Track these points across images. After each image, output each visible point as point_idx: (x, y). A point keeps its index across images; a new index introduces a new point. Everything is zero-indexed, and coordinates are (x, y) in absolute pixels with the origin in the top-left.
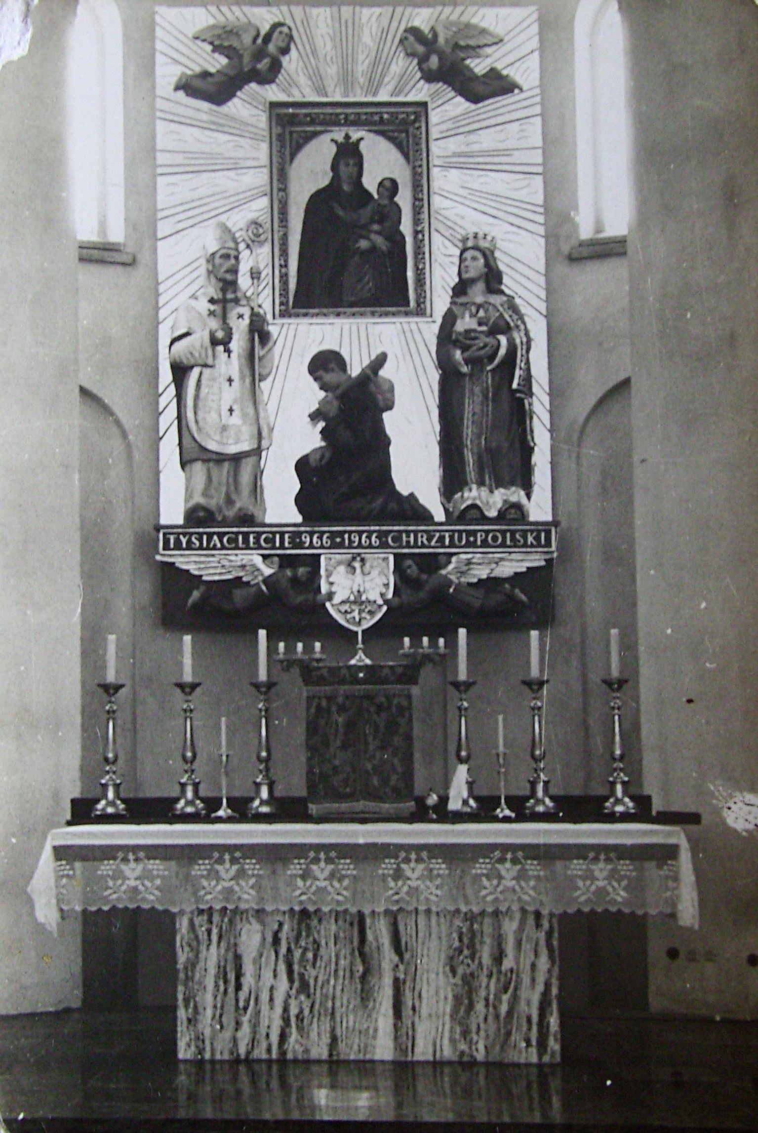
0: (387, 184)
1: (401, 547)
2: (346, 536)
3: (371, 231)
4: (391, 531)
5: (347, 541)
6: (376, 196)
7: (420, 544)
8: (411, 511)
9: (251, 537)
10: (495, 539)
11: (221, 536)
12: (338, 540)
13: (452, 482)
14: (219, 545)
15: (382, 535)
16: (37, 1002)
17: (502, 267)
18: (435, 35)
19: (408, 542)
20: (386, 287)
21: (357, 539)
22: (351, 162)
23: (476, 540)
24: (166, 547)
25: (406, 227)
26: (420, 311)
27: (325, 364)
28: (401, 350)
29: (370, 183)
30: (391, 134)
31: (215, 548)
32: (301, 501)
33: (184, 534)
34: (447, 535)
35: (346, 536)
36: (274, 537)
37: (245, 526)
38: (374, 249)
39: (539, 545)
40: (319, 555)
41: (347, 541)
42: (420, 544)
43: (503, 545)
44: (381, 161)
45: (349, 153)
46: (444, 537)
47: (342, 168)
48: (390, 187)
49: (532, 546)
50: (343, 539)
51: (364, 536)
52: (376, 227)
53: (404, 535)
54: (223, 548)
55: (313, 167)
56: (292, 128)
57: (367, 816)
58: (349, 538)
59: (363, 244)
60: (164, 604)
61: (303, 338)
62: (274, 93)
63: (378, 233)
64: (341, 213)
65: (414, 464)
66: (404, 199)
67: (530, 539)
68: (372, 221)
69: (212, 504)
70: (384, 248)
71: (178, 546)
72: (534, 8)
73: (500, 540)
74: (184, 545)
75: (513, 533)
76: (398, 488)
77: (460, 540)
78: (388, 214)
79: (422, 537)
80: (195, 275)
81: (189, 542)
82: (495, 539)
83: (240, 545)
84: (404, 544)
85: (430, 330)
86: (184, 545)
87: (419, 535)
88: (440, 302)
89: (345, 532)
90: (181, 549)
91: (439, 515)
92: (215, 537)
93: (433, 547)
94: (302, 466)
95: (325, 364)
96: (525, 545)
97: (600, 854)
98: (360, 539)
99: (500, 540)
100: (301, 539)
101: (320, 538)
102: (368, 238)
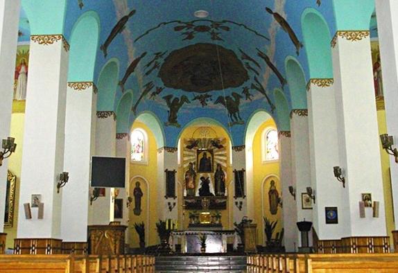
13: (216, 191)
20: (210, 170)
27: (202, 178)
45: (205, 154)
48: (210, 158)
56: (199, 152)
65: (212, 190)
88: (215, 172)
95: (202, 178)
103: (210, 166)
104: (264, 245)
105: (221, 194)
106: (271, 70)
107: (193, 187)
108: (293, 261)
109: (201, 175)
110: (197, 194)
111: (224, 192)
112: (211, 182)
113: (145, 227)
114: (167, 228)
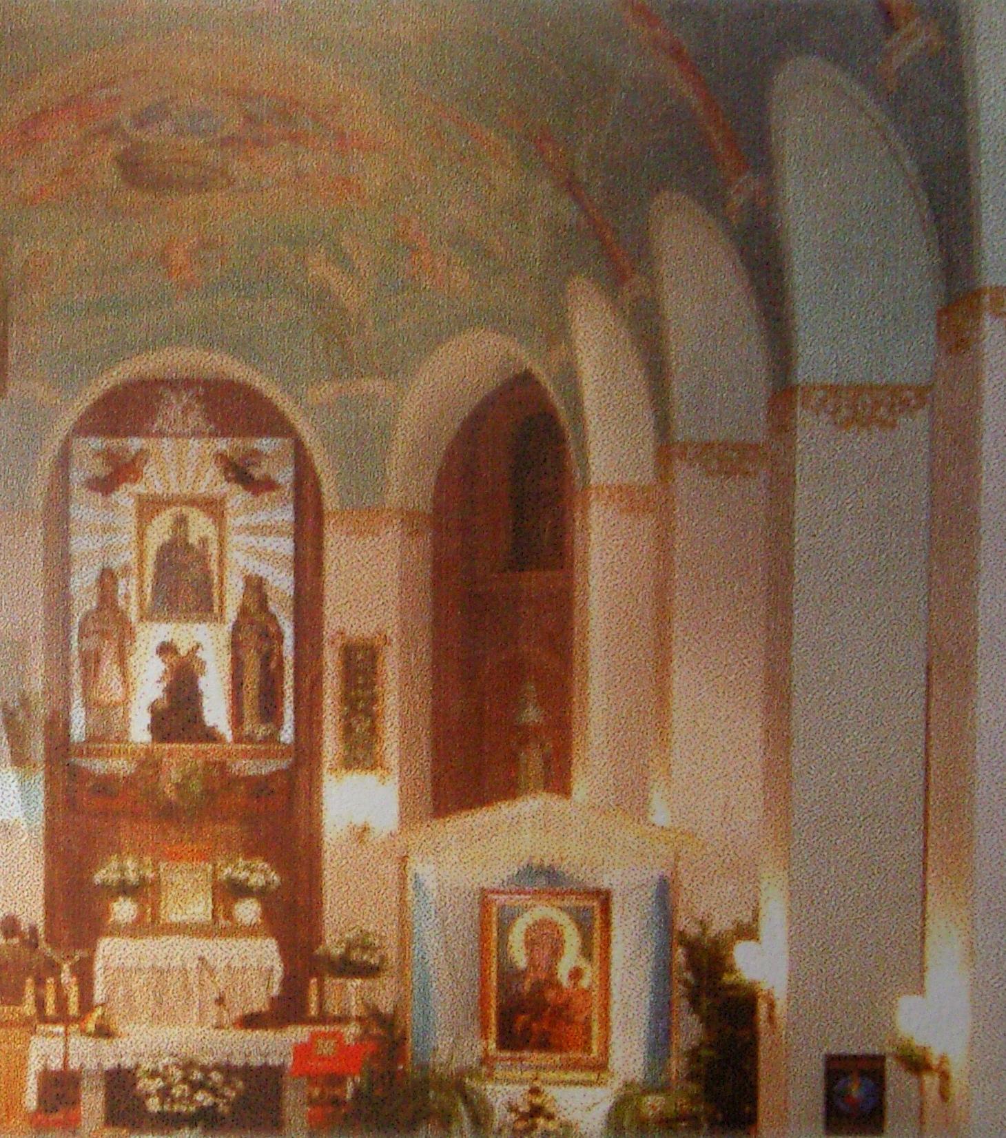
8: (211, 736)
13: (237, 720)
16: (622, 511)
20: (203, 605)
25: (214, 567)
26: (223, 621)
27: (166, 649)
28: (209, 642)
29: (193, 539)
44: (200, 527)
45: (181, 521)
48: (204, 541)
55: (160, 530)
56: (149, 507)
57: (597, 935)
61: (151, 635)
62: (139, 488)
65: (216, 710)
76: (206, 719)
78: (203, 558)
85: (228, 628)
88: (231, 614)
91: (229, 737)
94: (153, 709)
95: (166, 649)
97: (104, 886)
103: (207, 583)
104: (124, 823)
105: (261, 731)
106: (613, 1015)
107: (118, 695)
108: (649, 521)
109: (162, 632)
111: (279, 726)
112: (211, 667)
113: (238, 1061)
114: (4, 981)
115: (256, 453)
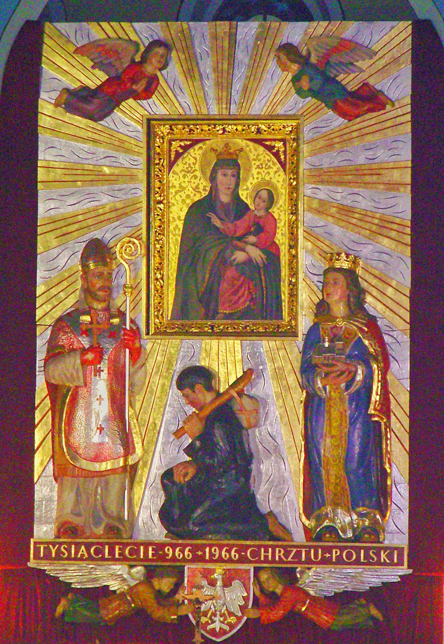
0: (264, 194)
1: (259, 561)
2: (207, 550)
3: (246, 243)
4: (249, 546)
5: (207, 555)
6: (252, 207)
7: (277, 558)
9: (117, 547)
10: (349, 555)
11: (88, 546)
12: (200, 553)
14: (86, 556)
15: (241, 549)
17: (364, 285)
18: (309, 55)
19: (266, 557)
21: (223, 553)
22: (229, 172)
23: (331, 558)
24: (37, 556)
25: (281, 239)
30: (268, 143)
31: (82, 559)
32: (165, 515)
33: (54, 544)
34: (303, 550)
35: (207, 550)
36: (260, 550)
37: (116, 539)
38: (249, 261)
39: (392, 564)
40: (184, 566)
41: (207, 555)
42: (277, 558)
43: (357, 562)
45: (229, 162)
46: (300, 552)
47: (220, 177)
49: (385, 564)
50: (204, 553)
51: (178, 549)
52: (252, 239)
53: (262, 550)
54: (91, 558)
55: (186, 185)
58: (210, 552)
59: (240, 256)
60: (111, 396)
63: (253, 245)
64: (217, 223)
65: (279, 482)
66: (281, 212)
67: (383, 556)
68: (248, 233)
69: (77, 521)
70: (259, 260)
71: (48, 556)
72: (410, 22)
73: (354, 557)
74: (53, 555)
75: (367, 550)
77: (316, 555)
78: (263, 228)
79: (280, 551)
80: (70, 289)
81: (58, 552)
82: (349, 555)
83: (107, 555)
84: (262, 559)
86: (53, 555)
87: (277, 550)
89: (206, 545)
90: (51, 559)
92: (83, 548)
93: (290, 562)
96: (379, 563)
98: (174, 552)
99: (354, 557)
100: (240, 555)
101: (229, 551)
102: (243, 250)
110: (148, 522)
115: (345, 45)
